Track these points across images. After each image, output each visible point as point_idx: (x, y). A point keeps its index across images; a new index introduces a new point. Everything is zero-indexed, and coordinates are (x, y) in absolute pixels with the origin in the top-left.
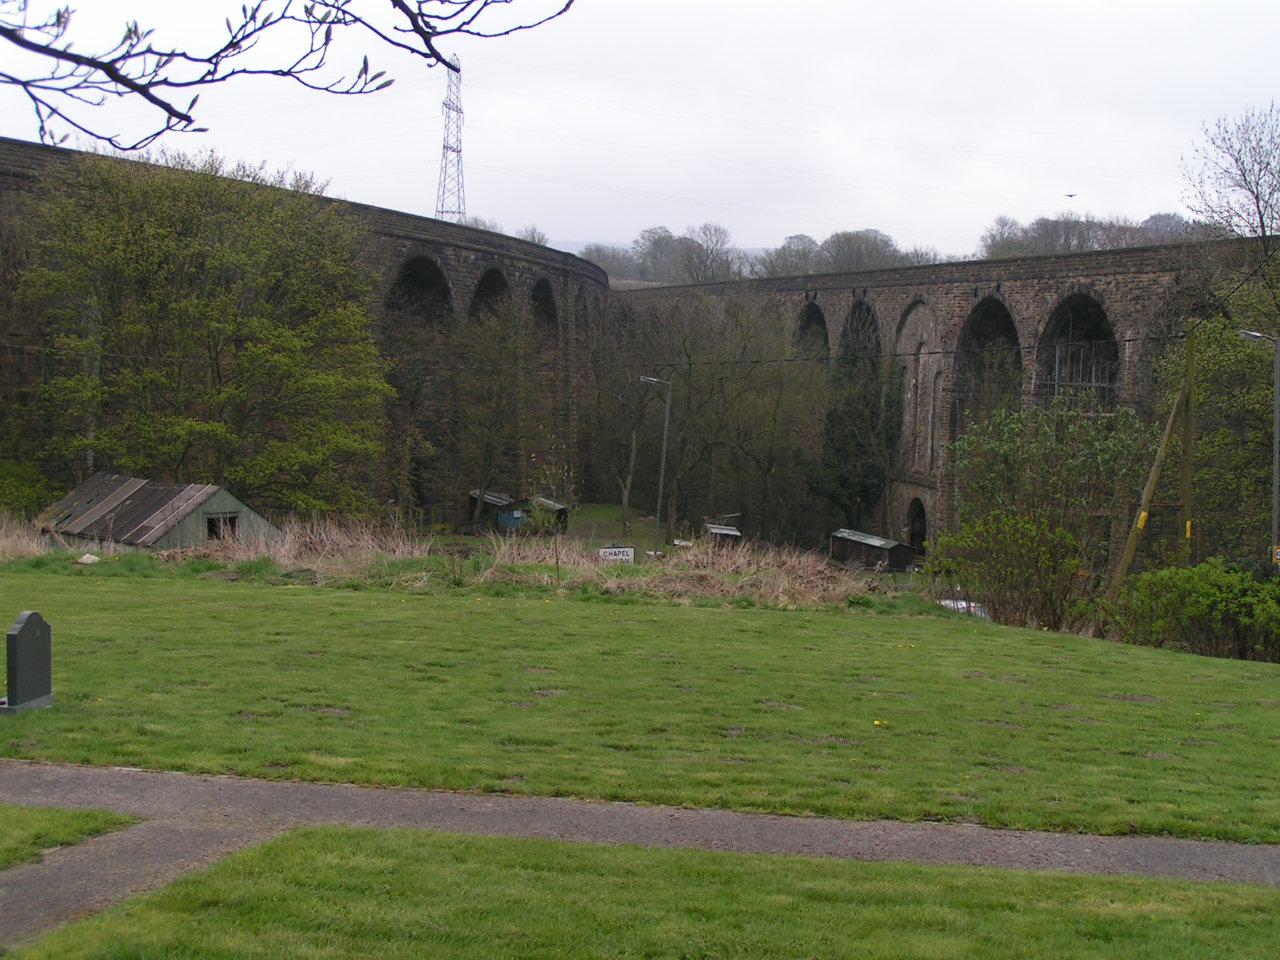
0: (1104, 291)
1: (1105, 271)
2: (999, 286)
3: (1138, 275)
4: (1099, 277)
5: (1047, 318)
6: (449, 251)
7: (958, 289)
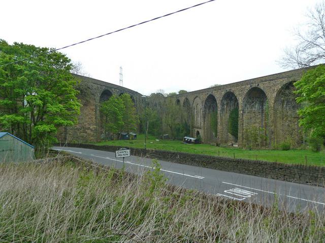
6: (113, 89)
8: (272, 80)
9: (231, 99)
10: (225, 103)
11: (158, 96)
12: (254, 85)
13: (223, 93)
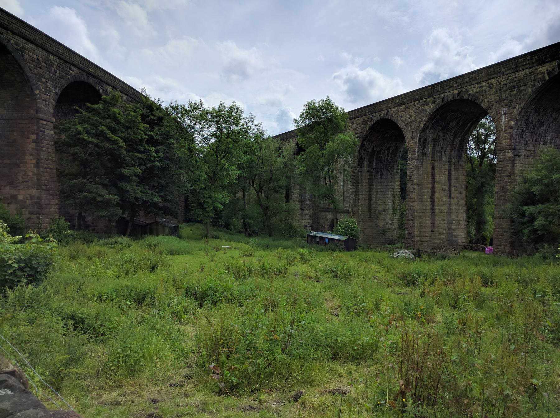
2: (388, 112)
4: (472, 86)
7: (359, 120)
10: (431, 136)
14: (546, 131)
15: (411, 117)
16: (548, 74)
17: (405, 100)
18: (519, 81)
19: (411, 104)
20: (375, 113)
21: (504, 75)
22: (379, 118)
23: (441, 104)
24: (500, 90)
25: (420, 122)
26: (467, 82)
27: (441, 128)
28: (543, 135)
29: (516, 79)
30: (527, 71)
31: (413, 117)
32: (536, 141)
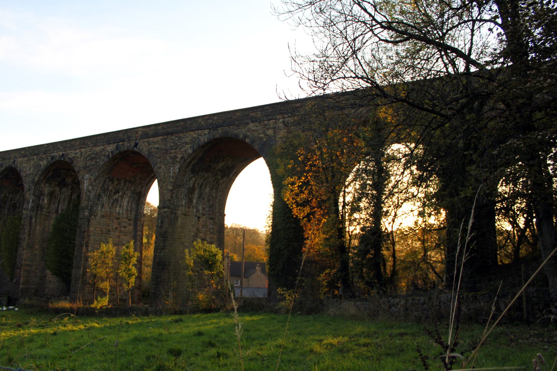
0: (73, 157)
1: (75, 148)
2: (14, 161)
3: (94, 148)
4: (71, 151)
5: (40, 173)
8: (172, 134)
9: (62, 184)
10: (47, 190)
11: (272, 183)
12: (126, 145)
13: (44, 163)
14: (122, 197)
15: (30, 169)
16: (112, 152)
17: (28, 153)
18: (96, 154)
19: (32, 157)
20: (6, 160)
21: (89, 147)
22: (8, 165)
23: (51, 162)
24: (86, 159)
25: (36, 175)
26: (68, 147)
27: (56, 183)
28: (119, 200)
29: (95, 152)
30: (101, 147)
31: (32, 169)
32: (112, 204)
